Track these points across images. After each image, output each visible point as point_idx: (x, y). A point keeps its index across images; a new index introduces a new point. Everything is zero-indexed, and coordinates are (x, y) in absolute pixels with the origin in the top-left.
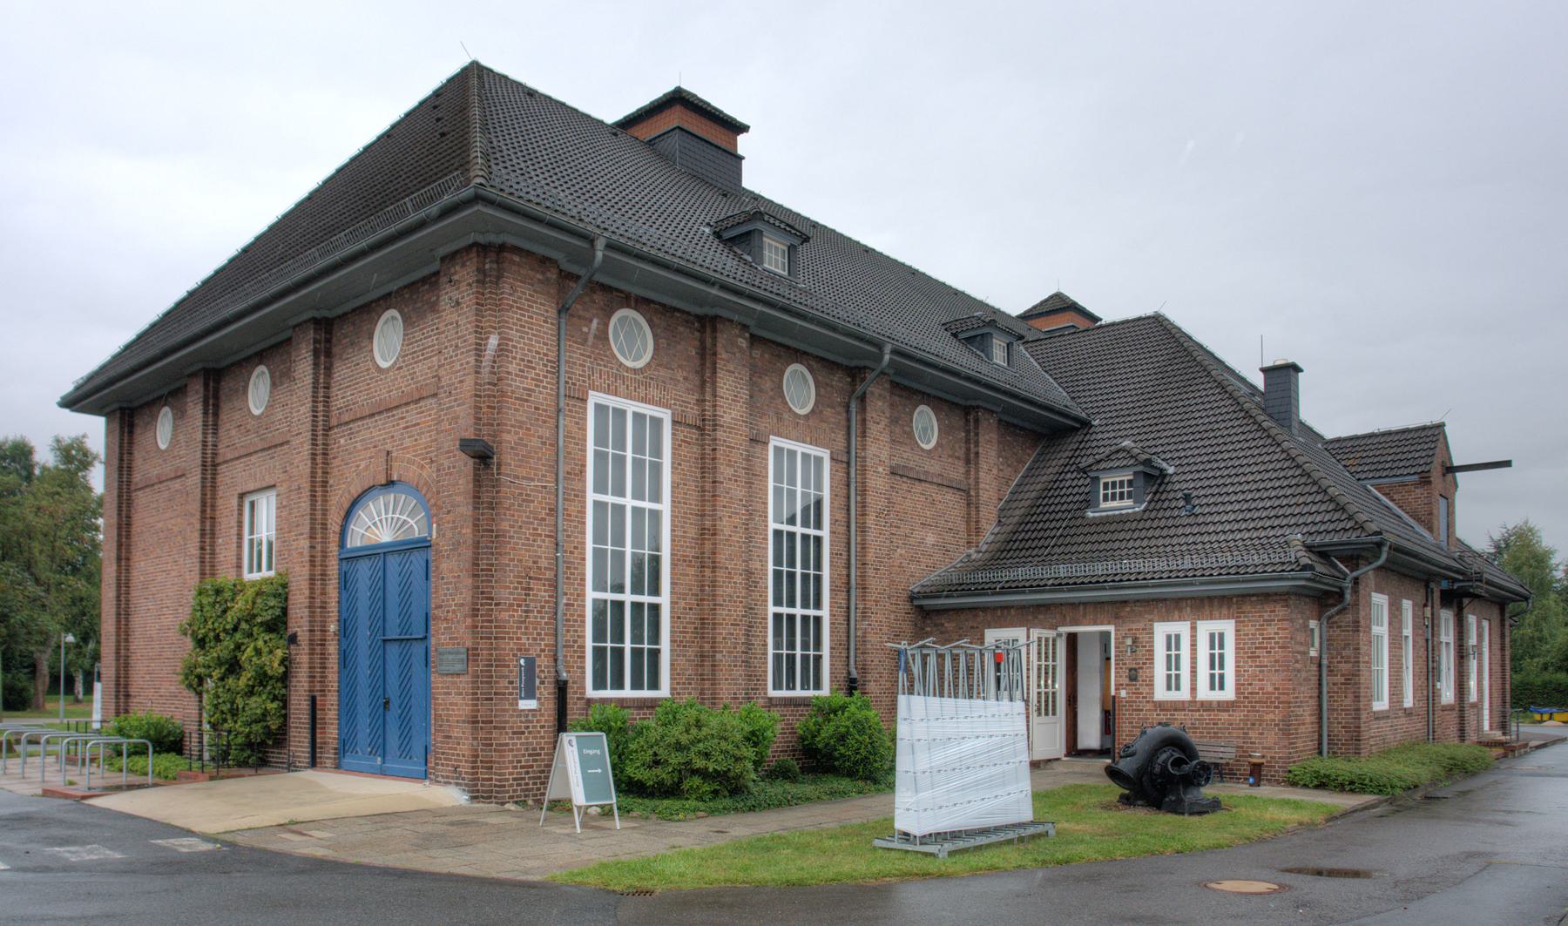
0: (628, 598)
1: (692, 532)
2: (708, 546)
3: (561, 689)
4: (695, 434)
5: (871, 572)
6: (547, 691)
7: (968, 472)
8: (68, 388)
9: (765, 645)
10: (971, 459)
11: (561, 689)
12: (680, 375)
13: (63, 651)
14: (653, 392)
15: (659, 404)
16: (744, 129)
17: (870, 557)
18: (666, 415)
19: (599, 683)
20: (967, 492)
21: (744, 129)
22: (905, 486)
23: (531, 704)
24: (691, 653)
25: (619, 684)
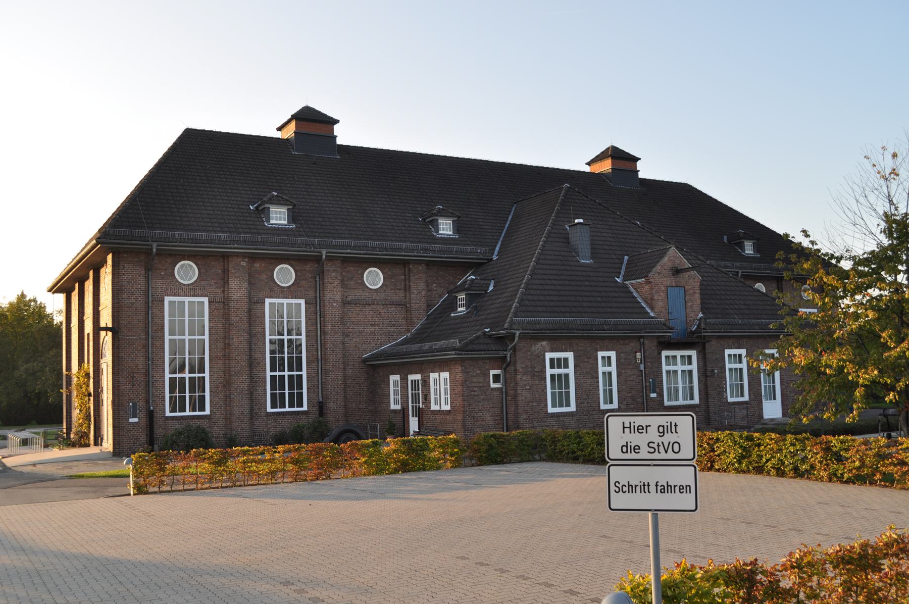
0: (187, 375)
1: (221, 345)
2: (227, 351)
3: (151, 415)
4: (221, 305)
5: (329, 352)
6: (143, 415)
7: (405, 296)
8: (50, 284)
9: (265, 390)
10: (407, 289)
11: (151, 415)
12: (212, 282)
13: (623, 272)
14: (200, 292)
15: (202, 296)
16: (337, 122)
17: (329, 345)
18: (206, 300)
19: (173, 410)
20: (405, 305)
21: (337, 122)
22: (358, 309)
23: (136, 420)
24: (221, 395)
25: (183, 409)
